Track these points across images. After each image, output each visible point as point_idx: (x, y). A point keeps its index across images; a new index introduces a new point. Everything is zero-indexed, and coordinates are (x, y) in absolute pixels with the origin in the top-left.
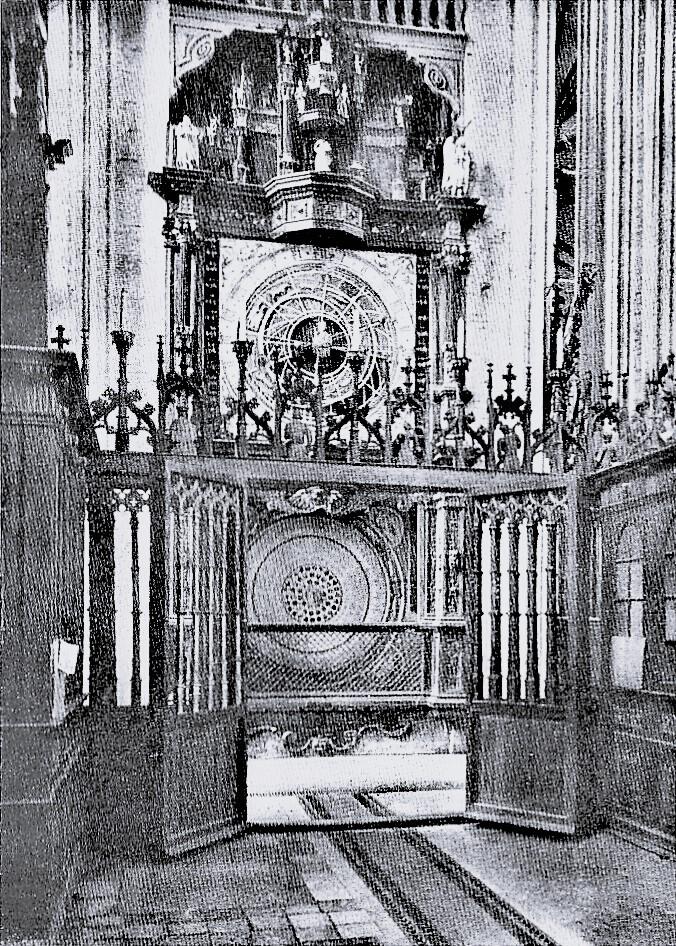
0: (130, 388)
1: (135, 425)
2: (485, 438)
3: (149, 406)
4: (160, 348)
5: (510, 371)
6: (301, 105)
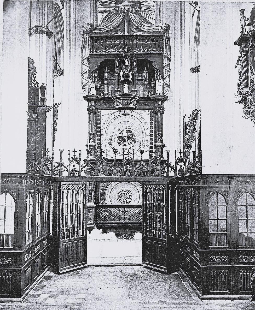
0: (63, 161)
1: (171, 170)
2: (68, 168)
3: (67, 165)
4: (176, 152)
5: (74, 150)
6: (121, 76)
